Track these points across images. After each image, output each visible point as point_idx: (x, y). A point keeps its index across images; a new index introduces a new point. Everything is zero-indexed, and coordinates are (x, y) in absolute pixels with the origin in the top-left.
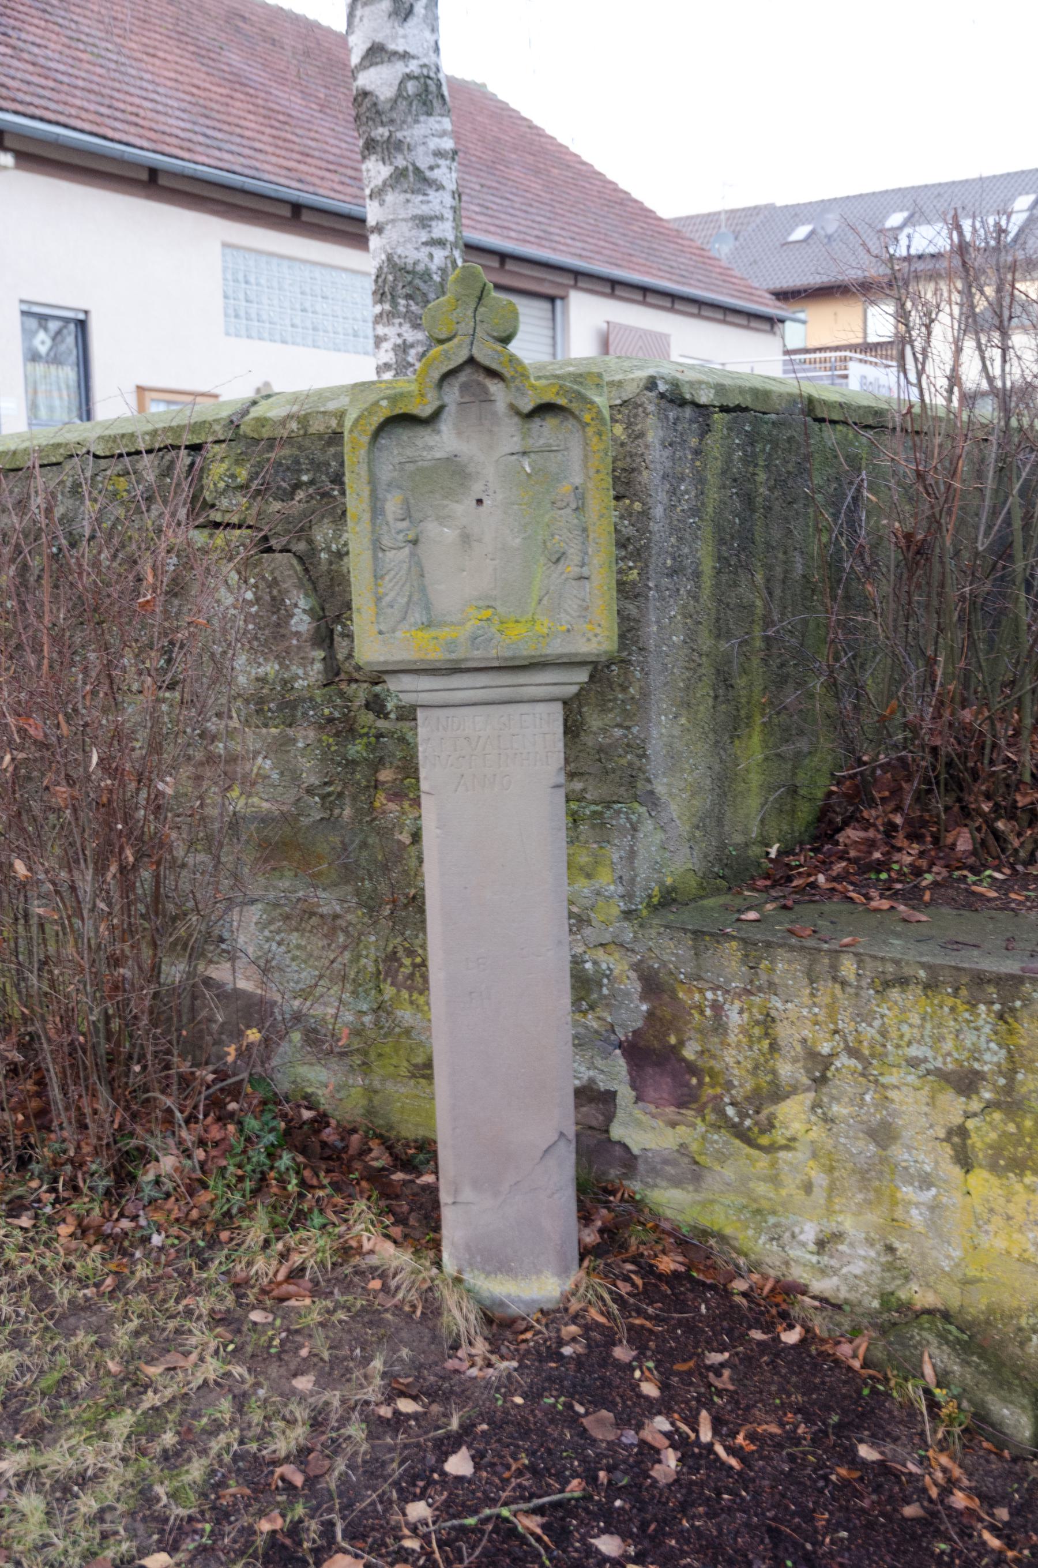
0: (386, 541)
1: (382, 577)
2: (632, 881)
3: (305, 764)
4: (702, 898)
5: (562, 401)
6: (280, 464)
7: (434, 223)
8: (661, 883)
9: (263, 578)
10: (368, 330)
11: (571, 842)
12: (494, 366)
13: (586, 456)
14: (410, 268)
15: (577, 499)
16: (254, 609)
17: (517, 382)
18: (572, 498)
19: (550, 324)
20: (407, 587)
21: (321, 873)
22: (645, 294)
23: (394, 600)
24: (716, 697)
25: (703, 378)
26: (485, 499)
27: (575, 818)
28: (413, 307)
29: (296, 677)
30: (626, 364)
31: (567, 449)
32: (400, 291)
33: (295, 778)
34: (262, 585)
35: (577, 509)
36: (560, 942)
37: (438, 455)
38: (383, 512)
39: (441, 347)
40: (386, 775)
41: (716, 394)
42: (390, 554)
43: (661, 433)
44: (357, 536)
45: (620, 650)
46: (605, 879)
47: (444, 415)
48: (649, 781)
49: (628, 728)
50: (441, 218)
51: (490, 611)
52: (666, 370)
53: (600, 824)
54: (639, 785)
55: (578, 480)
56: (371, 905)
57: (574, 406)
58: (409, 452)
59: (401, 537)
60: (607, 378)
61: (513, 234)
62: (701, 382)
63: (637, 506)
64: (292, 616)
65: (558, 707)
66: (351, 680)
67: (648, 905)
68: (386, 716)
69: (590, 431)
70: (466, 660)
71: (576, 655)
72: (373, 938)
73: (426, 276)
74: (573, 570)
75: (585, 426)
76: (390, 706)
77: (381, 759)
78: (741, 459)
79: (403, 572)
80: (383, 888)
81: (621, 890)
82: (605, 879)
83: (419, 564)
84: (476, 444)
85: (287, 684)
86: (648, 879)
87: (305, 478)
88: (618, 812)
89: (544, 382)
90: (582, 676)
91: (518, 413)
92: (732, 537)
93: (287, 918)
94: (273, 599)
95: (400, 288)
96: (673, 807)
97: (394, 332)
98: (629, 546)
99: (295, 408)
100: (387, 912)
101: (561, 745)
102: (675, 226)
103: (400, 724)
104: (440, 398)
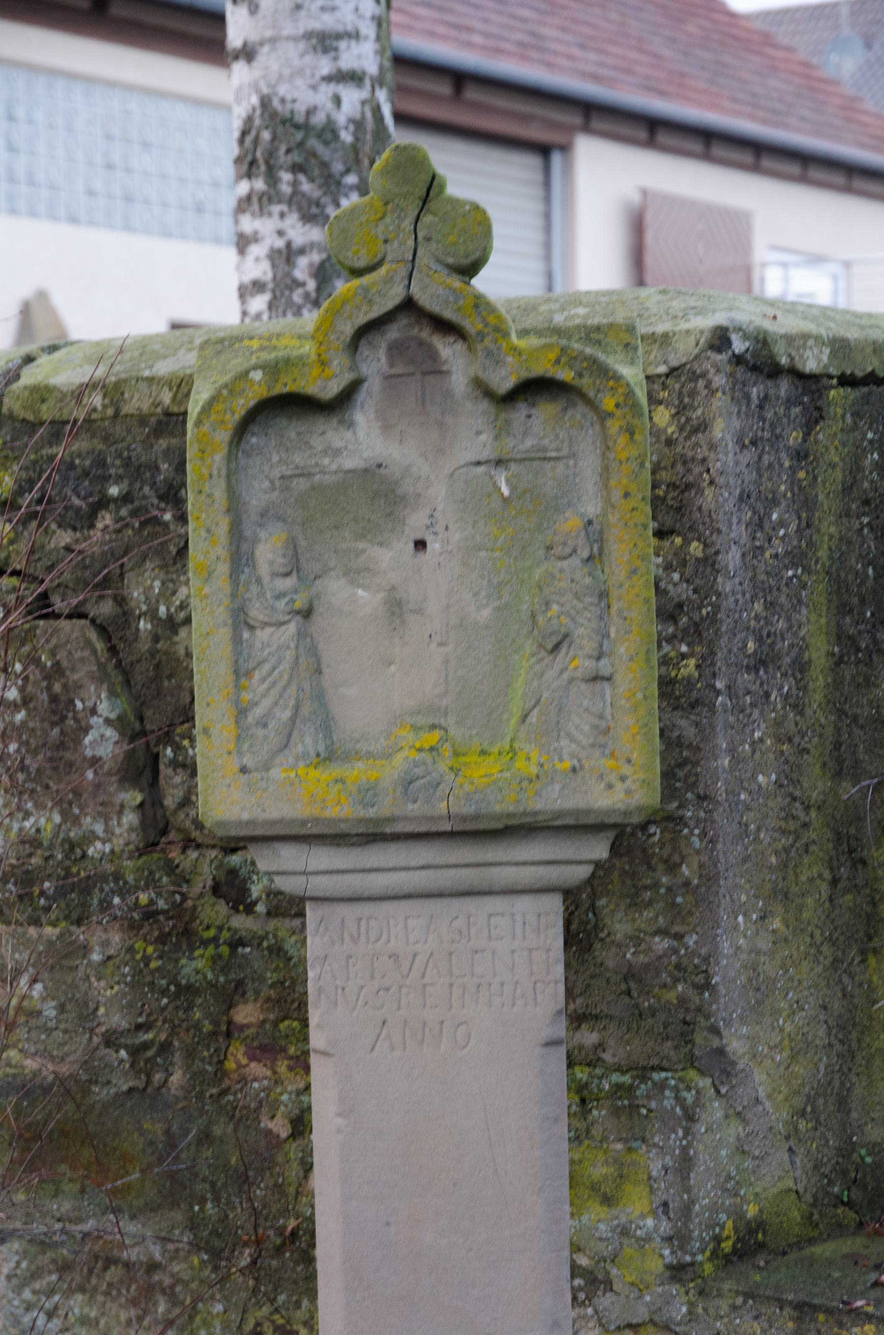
0: (256, 612)
1: (249, 674)
2: (686, 1211)
3: (104, 991)
4: (811, 1241)
5: (566, 375)
6: (71, 466)
7: (343, 45)
8: (738, 1215)
9: (37, 662)
10: (226, 226)
11: (576, 1139)
12: (448, 314)
13: (606, 469)
14: (300, 119)
15: (591, 542)
16: (20, 716)
17: (488, 341)
18: (581, 541)
19: (539, 192)
20: (293, 689)
21: (128, 1188)
22: (708, 142)
23: (269, 714)
24: (835, 882)
25: (810, 327)
26: (429, 539)
27: (583, 1098)
28: (306, 186)
29: (91, 837)
30: (677, 305)
31: (573, 455)
32: (282, 157)
33: (87, 1016)
34: (34, 674)
35: (590, 558)
36: (556, 1324)
37: (350, 463)
38: (251, 560)
39: (356, 282)
40: (246, 1014)
41: (833, 354)
42: (263, 635)
43: (736, 424)
44: (205, 593)
45: (665, 798)
46: (637, 1207)
47: (361, 396)
48: (715, 1031)
49: (679, 937)
50: (355, 36)
51: (437, 734)
52: (745, 314)
53: (627, 1107)
54: (698, 1038)
55: (592, 509)
56: (215, 1246)
57: (586, 383)
58: (299, 459)
59: (282, 604)
60: (643, 329)
61: (477, 39)
62: (805, 337)
63: (696, 548)
64: (86, 730)
65: (555, 905)
66: (188, 843)
67: (714, 1254)
68: (249, 909)
69: (613, 425)
70: (392, 819)
71: (588, 812)
72: (219, 1308)
73: (329, 132)
74: (582, 664)
75: (604, 417)
76: (256, 890)
77: (240, 983)
78: (876, 465)
79: (285, 666)
80: (239, 1216)
81: (665, 1227)
82: (637, 1207)
83: (314, 652)
84: (419, 447)
85: (74, 849)
86: (714, 1208)
87: (114, 491)
88: (662, 1086)
89: (534, 341)
90: (598, 849)
91: (488, 393)
92: (863, 601)
93: (64, 1268)
94: (54, 699)
95: (283, 154)
96: (759, 1076)
97: (271, 228)
98: (682, 618)
99: (101, 372)
100: (245, 1261)
101: (560, 969)
102: (758, 25)
103: (272, 924)
104: (354, 367)
